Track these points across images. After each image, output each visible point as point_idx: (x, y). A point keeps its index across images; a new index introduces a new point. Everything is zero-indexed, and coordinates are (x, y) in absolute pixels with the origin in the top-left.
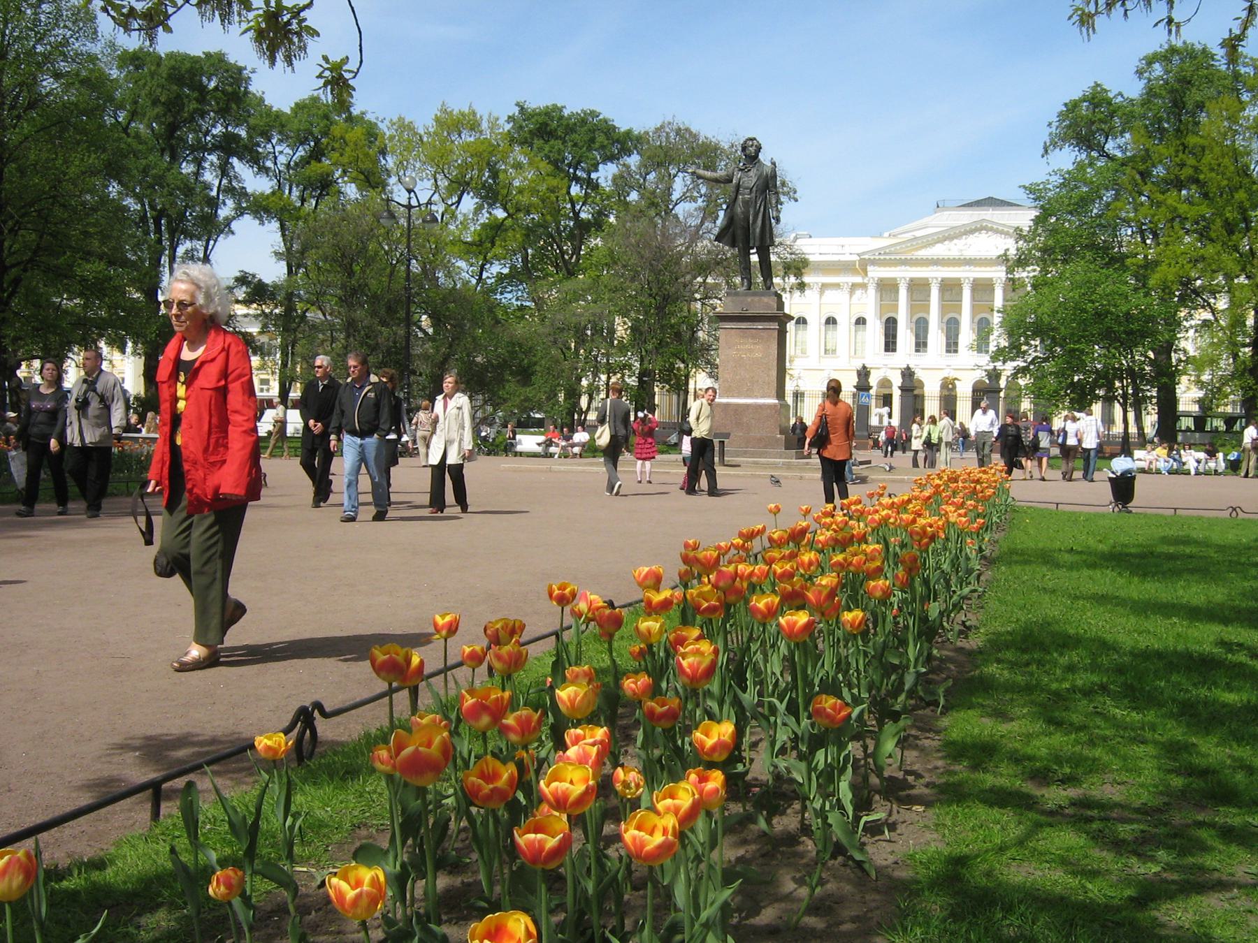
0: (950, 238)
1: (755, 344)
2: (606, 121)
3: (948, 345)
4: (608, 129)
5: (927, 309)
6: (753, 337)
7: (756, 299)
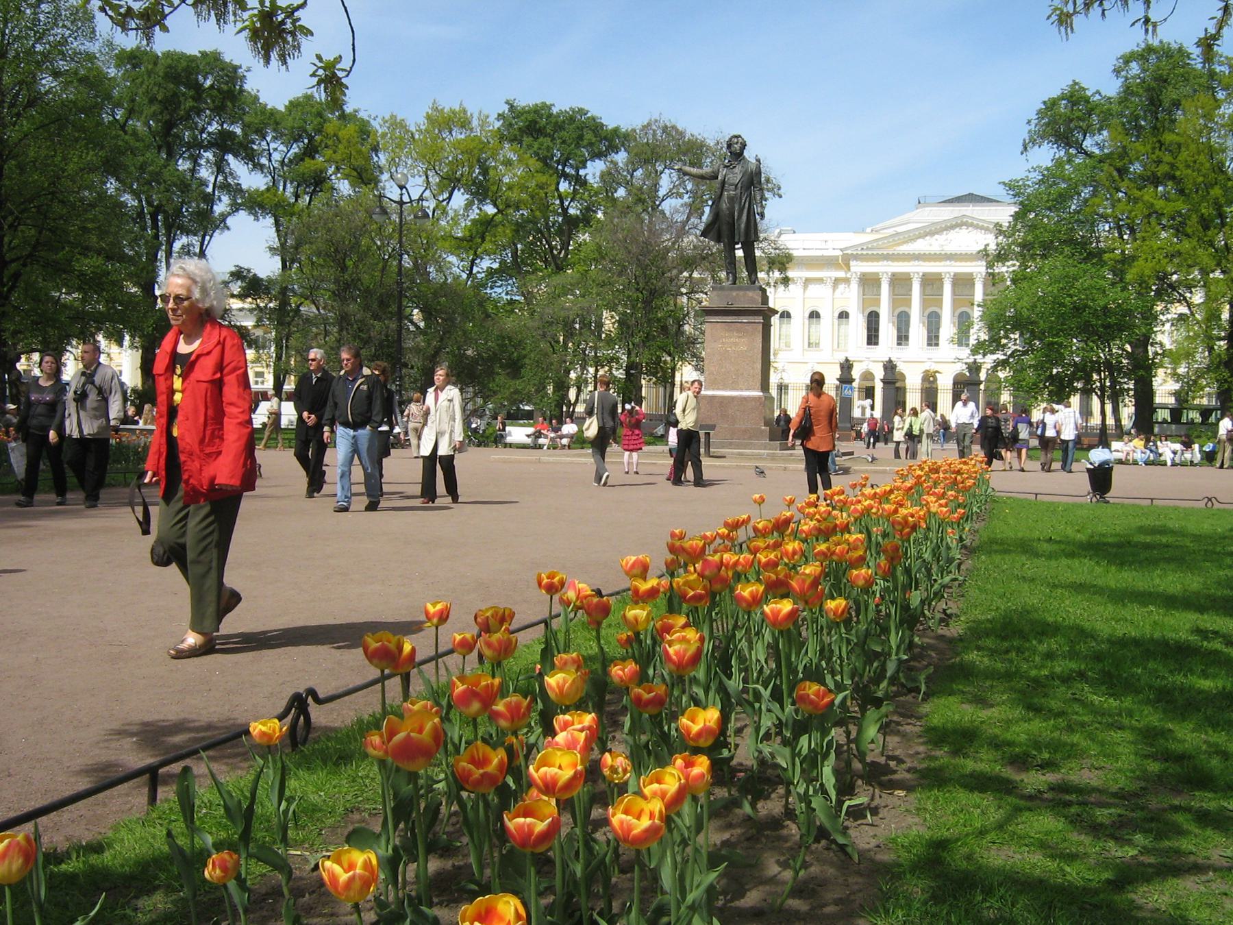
0: (932, 234)
1: (740, 337)
2: (594, 119)
3: (929, 338)
4: (596, 127)
5: (908, 303)
6: (738, 331)
7: (741, 293)
